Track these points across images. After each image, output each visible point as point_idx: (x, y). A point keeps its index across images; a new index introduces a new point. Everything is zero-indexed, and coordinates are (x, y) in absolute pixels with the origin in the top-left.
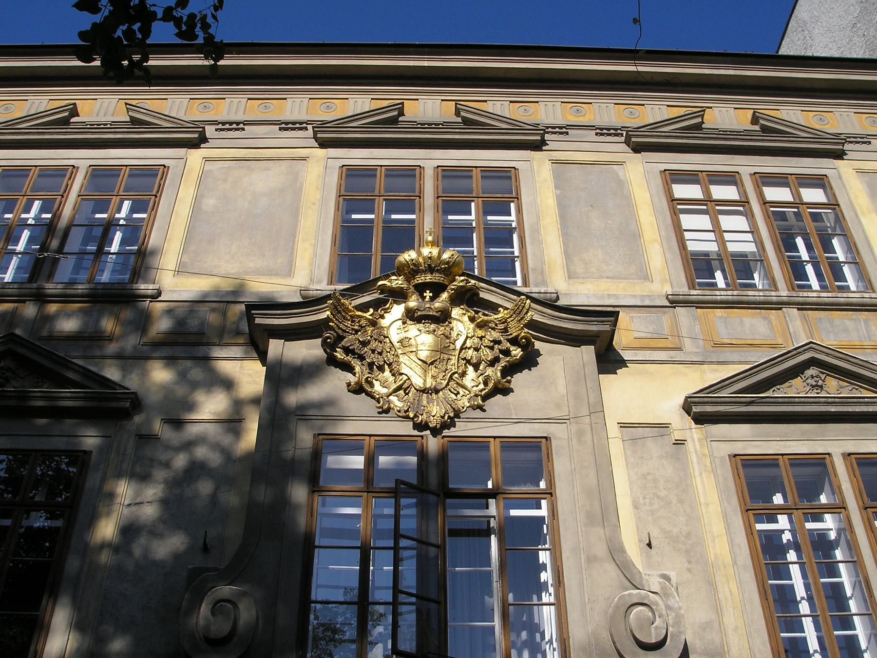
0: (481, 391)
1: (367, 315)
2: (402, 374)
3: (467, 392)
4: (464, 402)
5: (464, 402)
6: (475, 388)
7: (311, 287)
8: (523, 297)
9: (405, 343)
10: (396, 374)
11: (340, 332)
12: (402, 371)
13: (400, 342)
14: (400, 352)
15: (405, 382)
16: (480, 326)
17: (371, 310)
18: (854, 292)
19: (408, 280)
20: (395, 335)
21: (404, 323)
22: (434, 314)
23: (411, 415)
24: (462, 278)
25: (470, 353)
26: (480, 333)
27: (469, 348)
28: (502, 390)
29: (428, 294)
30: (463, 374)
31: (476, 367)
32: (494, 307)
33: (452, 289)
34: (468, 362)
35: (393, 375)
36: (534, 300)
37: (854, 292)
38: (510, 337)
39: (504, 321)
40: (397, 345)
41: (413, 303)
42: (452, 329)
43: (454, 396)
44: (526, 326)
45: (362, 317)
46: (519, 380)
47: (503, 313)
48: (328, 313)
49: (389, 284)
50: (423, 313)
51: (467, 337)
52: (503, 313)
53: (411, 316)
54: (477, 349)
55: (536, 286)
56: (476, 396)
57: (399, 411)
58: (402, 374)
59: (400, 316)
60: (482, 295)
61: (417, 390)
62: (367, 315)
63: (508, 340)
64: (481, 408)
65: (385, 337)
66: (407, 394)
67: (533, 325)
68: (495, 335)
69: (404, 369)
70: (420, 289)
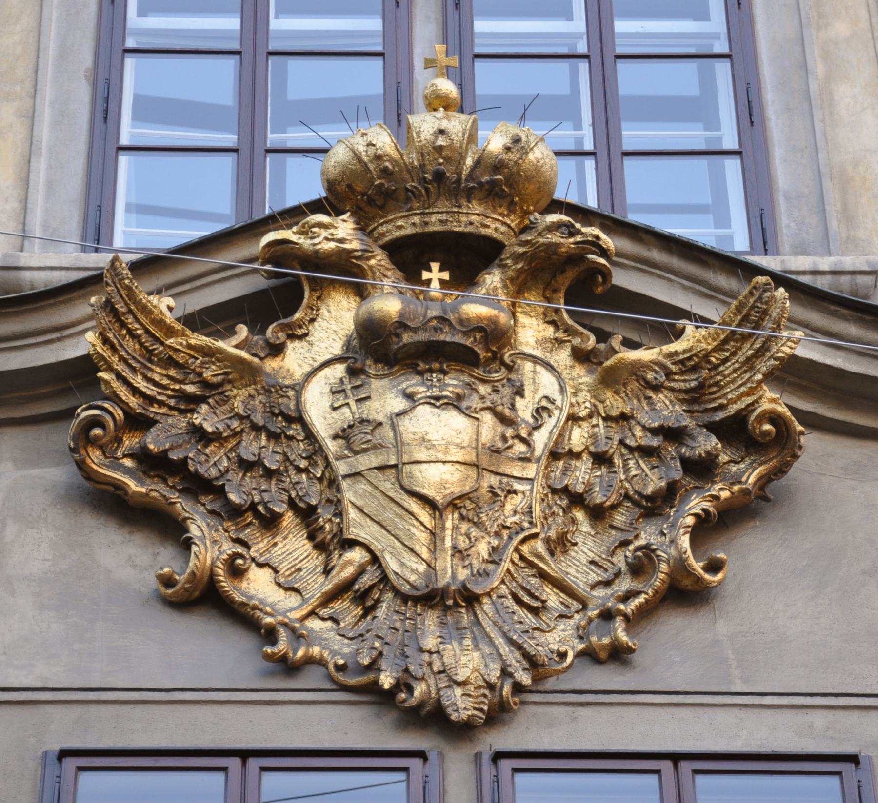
0: (626, 597)
1: (227, 346)
2: (351, 544)
3: (575, 605)
4: (560, 638)
5: (560, 638)
6: (600, 592)
7: (25, 259)
8: (761, 279)
9: (358, 439)
10: (330, 544)
11: (133, 402)
12: (353, 533)
13: (343, 435)
14: (342, 468)
15: (361, 571)
16: (611, 379)
17: (243, 331)
18: (428, 686)
19: (363, 226)
20: (320, 409)
21: (352, 372)
22: (458, 339)
23: (386, 681)
24: (553, 218)
25: (582, 474)
26: (615, 404)
27: (578, 456)
28: (685, 593)
29: (435, 274)
30: (561, 544)
31: (598, 514)
32: (663, 321)
33: (517, 257)
34: (576, 500)
35: (321, 547)
36: (802, 291)
37: (428, 686)
38: (720, 416)
39: (690, 364)
40: (332, 447)
41: (388, 304)
42: (520, 392)
43: (530, 619)
44: (771, 377)
45: (208, 353)
46: (750, 555)
47: (692, 338)
48: (90, 336)
49: (305, 242)
50: (422, 337)
51: (573, 418)
52: (692, 338)
53: (377, 349)
54: (601, 459)
55: (801, 250)
56: (607, 615)
57: (340, 668)
58: (351, 544)
59: (337, 349)
60: (622, 279)
61: (405, 598)
62: (227, 346)
63: (713, 428)
64: (618, 655)
65: (289, 420)
66: (368, 611)
67: (794, 374)
68: (667, 409)
69: (359, 527)
70: (409, 256)
